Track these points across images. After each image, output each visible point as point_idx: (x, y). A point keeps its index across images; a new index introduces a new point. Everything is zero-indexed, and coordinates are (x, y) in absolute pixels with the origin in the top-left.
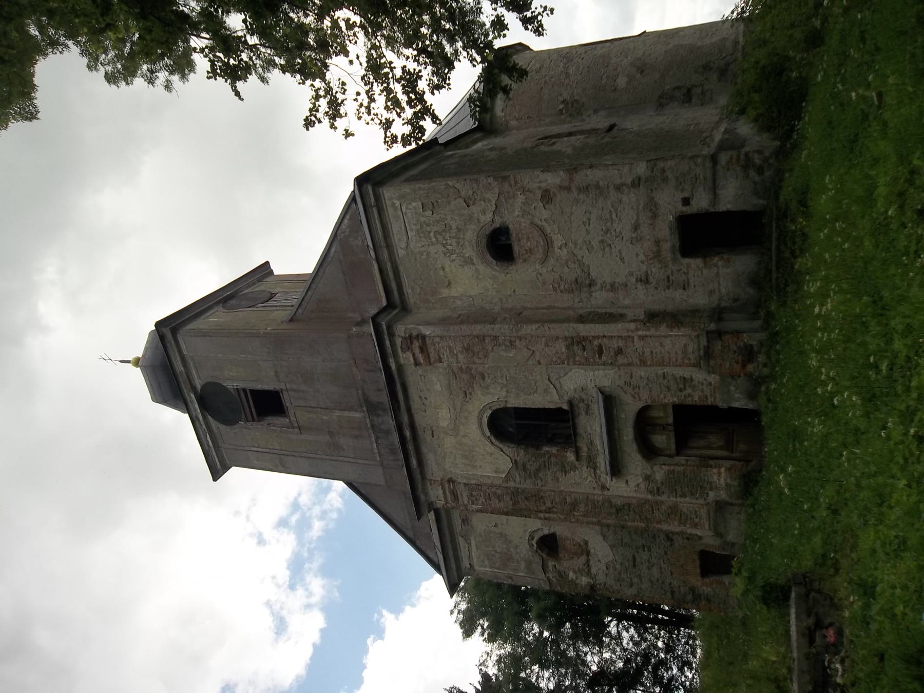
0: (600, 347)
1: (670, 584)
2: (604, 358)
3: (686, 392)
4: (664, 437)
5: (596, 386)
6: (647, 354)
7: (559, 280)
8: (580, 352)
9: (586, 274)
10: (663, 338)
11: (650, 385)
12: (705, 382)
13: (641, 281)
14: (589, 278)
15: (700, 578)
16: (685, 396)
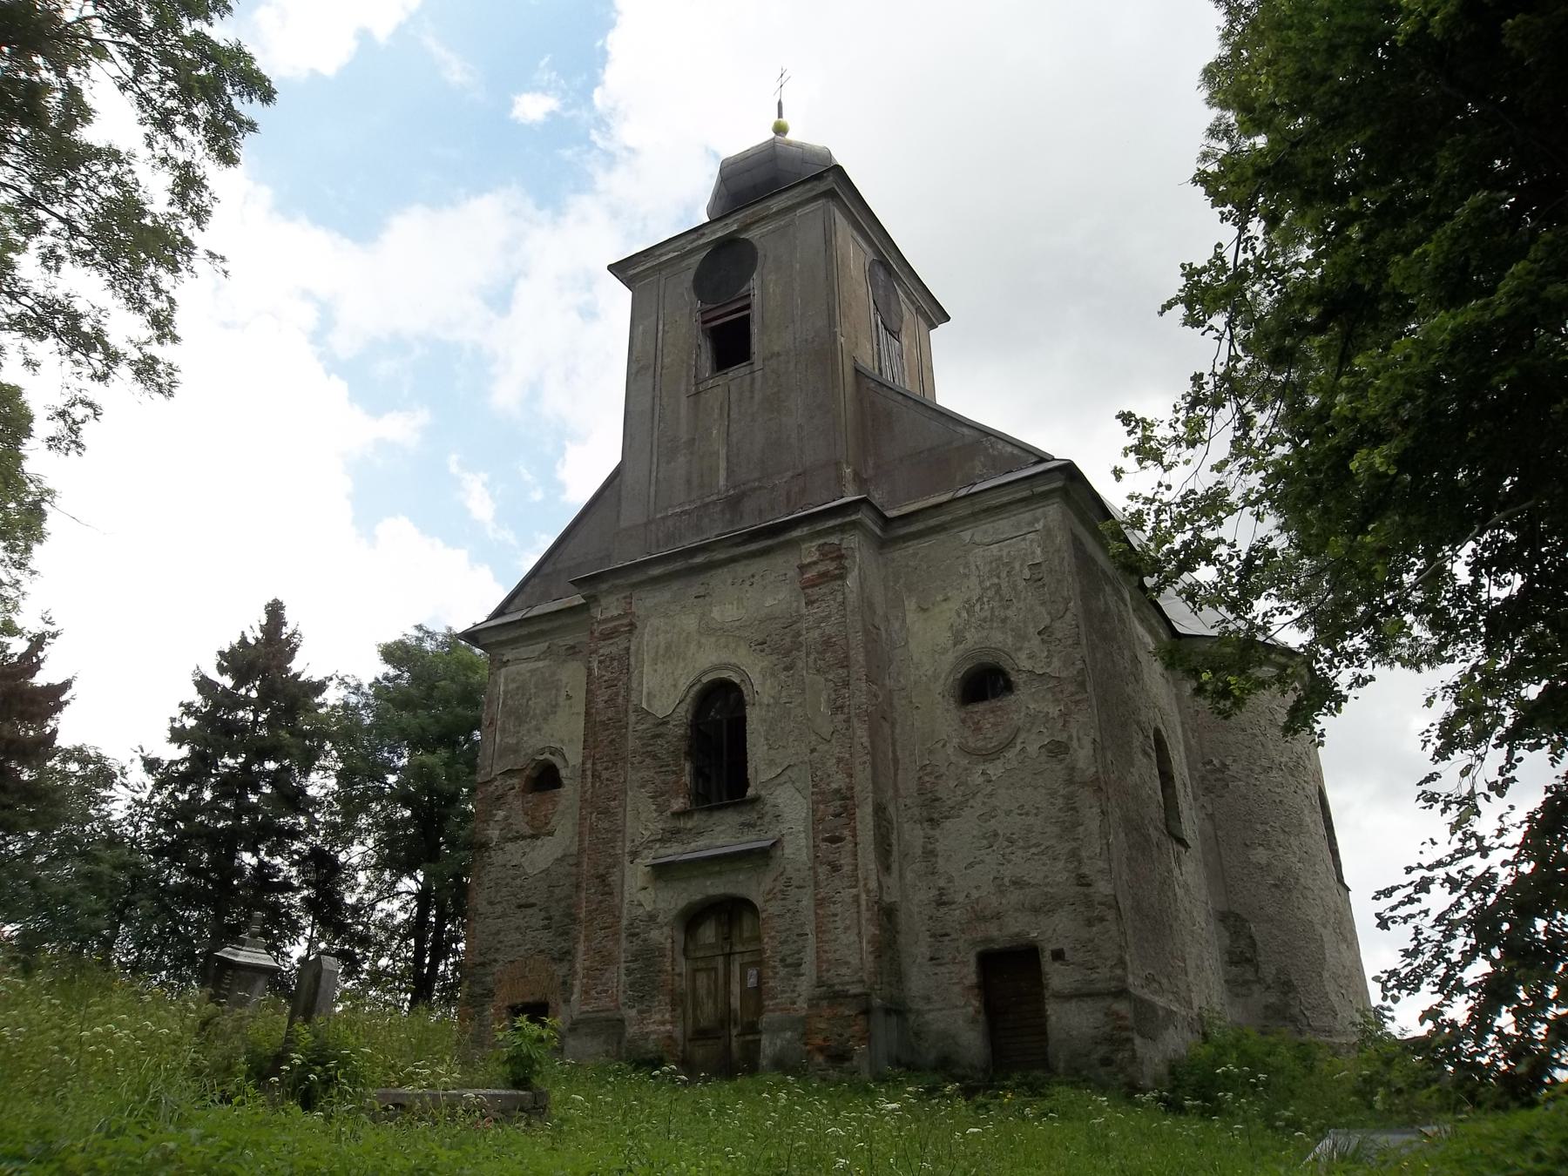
0: (840, 839)
1: (495, 961)
2: (824, 846)
4: (713, 940)
8: (831, 810)
13: (941, 895)
15: (507, 1004)
16: (775, 967)
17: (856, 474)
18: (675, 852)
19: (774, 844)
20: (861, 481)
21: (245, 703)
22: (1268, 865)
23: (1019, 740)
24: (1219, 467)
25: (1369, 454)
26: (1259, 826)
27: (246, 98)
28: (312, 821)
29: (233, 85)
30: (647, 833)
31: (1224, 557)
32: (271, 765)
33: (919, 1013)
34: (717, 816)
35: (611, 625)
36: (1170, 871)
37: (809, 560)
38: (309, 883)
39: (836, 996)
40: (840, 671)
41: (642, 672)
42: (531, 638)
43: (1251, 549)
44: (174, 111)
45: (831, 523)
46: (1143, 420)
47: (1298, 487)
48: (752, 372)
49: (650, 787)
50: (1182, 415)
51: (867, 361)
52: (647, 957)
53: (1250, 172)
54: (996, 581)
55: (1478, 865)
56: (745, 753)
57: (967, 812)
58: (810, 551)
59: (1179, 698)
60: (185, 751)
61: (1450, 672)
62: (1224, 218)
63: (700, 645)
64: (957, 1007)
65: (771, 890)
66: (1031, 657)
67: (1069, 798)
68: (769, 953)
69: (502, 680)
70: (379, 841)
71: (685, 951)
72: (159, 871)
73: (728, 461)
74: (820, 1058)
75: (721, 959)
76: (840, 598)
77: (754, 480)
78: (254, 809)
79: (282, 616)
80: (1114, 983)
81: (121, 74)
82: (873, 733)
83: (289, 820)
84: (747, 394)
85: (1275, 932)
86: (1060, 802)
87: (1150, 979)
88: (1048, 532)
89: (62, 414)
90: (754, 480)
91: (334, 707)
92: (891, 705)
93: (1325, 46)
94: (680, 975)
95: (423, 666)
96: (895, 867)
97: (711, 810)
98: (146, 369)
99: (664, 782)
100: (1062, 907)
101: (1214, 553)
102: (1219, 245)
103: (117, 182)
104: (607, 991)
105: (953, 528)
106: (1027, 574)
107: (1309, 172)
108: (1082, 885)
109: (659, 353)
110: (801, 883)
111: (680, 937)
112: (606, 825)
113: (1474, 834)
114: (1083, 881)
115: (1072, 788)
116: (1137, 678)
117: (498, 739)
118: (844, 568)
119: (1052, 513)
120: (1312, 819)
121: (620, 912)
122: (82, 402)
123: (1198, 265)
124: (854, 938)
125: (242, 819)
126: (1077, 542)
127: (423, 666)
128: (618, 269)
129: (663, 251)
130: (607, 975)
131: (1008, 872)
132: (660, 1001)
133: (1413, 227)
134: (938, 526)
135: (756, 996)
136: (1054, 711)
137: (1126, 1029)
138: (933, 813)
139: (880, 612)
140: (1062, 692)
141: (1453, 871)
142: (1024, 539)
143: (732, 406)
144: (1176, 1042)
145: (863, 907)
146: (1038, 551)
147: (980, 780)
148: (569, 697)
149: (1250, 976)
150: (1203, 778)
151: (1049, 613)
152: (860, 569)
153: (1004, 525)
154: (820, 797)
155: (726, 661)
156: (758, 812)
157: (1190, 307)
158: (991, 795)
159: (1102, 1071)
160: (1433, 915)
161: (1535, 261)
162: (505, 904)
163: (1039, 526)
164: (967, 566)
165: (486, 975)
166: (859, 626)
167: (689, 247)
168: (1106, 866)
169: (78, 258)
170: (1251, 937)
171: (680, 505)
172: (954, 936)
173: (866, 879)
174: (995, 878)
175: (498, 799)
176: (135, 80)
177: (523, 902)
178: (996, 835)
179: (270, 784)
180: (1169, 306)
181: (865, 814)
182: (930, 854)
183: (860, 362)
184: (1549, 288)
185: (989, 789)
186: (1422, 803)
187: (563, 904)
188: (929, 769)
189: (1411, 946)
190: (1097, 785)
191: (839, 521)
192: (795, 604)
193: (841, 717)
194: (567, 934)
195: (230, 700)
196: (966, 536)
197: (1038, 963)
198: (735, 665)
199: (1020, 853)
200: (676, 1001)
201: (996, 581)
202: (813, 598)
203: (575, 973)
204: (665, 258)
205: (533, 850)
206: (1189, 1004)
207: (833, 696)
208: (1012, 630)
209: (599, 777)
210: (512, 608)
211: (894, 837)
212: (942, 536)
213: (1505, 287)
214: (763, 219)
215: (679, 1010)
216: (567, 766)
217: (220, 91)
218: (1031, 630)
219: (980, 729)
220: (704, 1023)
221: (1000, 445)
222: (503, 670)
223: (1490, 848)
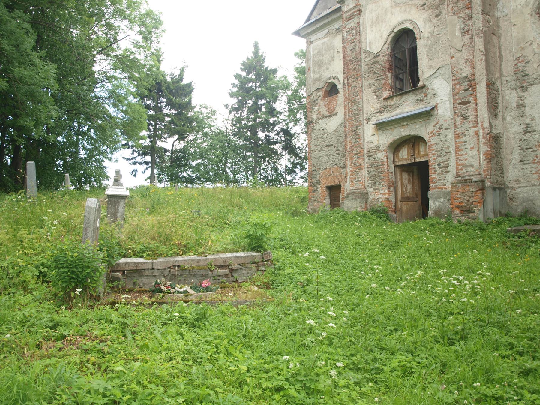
0: (468, 102)
1: (320, 169)
2: (459, 107)
3: (438, 169)
4: (407, 157)
5: (437, 104)
6: (464, 138)
7: (527, 61)
8: (463, 88)
9: (532, 82)
10: (477, 149)
11: (441, 143)
12: (446, 181)
13: (527, 127)
14: (529, 85)
16: (435, 168)
18: (386, 117)
19: (433, 109)
21: (251, 81)
30: (373, 109)
33: (512, 188)
34: (405, 97)
35: (350, 13)
60: (235, 100)
63: (392, 14)
64: (535, 185)
65: (432, 132)
69: (311, 50)
74: (457, 211)
82: (487, 43)
92: (498, 26)
94: (392, 173)
104: (360, 181)
110: (448, 127)
111: (391, 156)
112: (355, 108)
121: (364, 146)
124: (475, 152)
130: (360, 174)
132: (383, 185)
145: (481, 137)
154: (457, 81)
162: (321, 146)
165: (317, 174)
172: (535, 149)
173: (482, 122)
175: (315, 102)
177: (328, 144)
182: (521, 106)
188: (521, 59)
193: (467, 37)
209: (351, 86)
211: (500, 98)
220: (407, 194)
222: (312, 46)
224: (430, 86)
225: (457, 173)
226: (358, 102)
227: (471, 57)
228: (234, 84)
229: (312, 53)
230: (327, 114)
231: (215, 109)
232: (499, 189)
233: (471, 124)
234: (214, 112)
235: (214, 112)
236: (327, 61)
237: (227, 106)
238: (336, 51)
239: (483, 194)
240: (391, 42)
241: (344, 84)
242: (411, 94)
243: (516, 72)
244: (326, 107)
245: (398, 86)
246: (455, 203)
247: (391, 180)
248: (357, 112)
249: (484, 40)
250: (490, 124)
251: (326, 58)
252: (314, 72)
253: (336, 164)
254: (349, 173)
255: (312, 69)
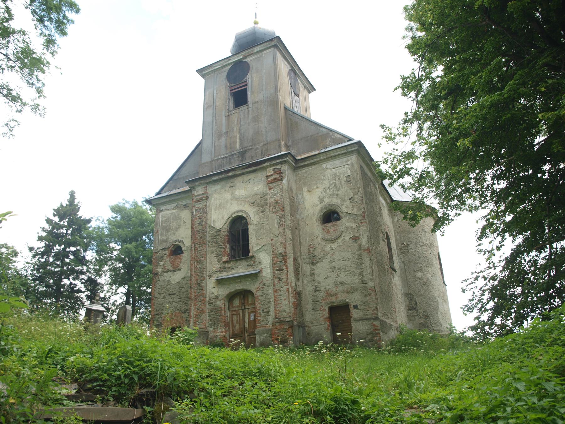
0: (282, 270)
1: (162, 313)
2: (276, 272)
4: (238, 305)
6: (280, 293)
8: (279, 260)
12: (267, 322)
13: (316, 288)
16: (260, 313)
17: (286, 144)
18: (224, 275)
19: (259, 272)
20: (287, 147)
21: (62, 227)
22: (421, 278)
23: (343, 236)
24: (414, 143)
25: (463, 141)
26: (418, 265)
27: (70, 12)
28: (88, 268)
29: (66, 7)
30: (214, 269)
31: (413, 174)
32: (73, 249)
33: (309, 327)
34: (239, 262)
35: (201, 196)
36: (391, 279)
37: (270, 174)
38: (88, 290)
39: (282, 322)
40: (281, 212)
41: (211, 213)
42: (170, 202)
43: (422, 171)
44: (44, 16)
45: (278, 161)
46: (388, 127)
47: (440, 151)
48: (248, 108)
49: (215, 253)
50: (401, 126)
51: (288, 105)
52: (216, 311)
53: (424, 46)
54: (335, 181)
55: (492, 272)
56: (248, 241)
57: (325, 260)
58: (270, 171)
59: (393, 222)
60: (43, 244)
61: (484, 212)
62: (415, 60)
63: (231, 204)
64: (321, 325)
65: (258, 287)
66: (347, 207)
67: (359, 255)
68: (258, 308)
69: (161, 217)
70: (111, 275)
71: (229, 308)
72: (36, 286)
73: (240, 139)
75: (241, 311)
76: (281, 187)
77: (250, 146)
78: (68, 264)
79: (74, 196)
80: (374, 315)
81: (26, 3)
82: (293, 234)
83: (80, 268)
84: (247, 116)
85: (423, 299)
86: (356, 256)
87: (385, 314)
88: (352, 165)
89: (7, 125)
90: (250, 146)
91: (95, 228)
92: (299, 224)
93: (450, 6)
94: (227, 316)
95: (125, 213)
96: (301, 279)
97: (237, 260)
98: (36, 108)
99: (220, 251)
100: (357, 291)
101: (410, 172)
102: (413, 69)
103: (24, 41)
105: (319, 163)
106: (345, 179)
107: (443, 47)
108: (364, 284)
109: (215, 101)
110: (269, 285)
111: (227, 304)
112: (200, 266)
113: (492, 262)
114: (364, 282)
115: (360, 252)
116: (381, 215)
117: (160, 238)
118: (282, 177)
119: (354, 158)
120: (436, 263)
121: (206, 296)
122: (13, 120)
123: (406, 76)
124: (287, 303)
125: (63, 268)
126: (361, 167)
127: (125, 213)
128: (200, 71)
129: (216, 65)
130: (202, 317)
131: (339, 280)
133: (478, 67)
134: (314, 162)
135: (254, 323)
136: (354, 225)
137: (378, 330)
138: (313, 260)
139: (294, 192)
140: (357, 219)
141: (485, 274)
142: (344, 167)
143: (241, 120)
144: (393, 334)
145: (290, 293)
146: (349, 171)
147: (329, 249)
148: (184, 222)
149: (415, 314)
150: (401, 249)
151: (353, 193)
152: (288, 177)
153: (337, 162)
154: (275, 255)
155: (241, 209)
156: (253, 261)
157: (403, 90)
158: (333, 254)
159: (370, 343)
160: (479, 288)
161: (516, 80)
163: (349, 163)
164: (324, 176)
166: (287, 197)
167: (225, 64)
168: (372, 277)
169: (9, 69)
170: (415, 301)
171: (223, 155)
172: (321, 301)
173: (291, 283)
174: (334, 282)
175: (161, 258)
176: (30, 5)
177: (171, 293)
178: (335, 267)
179: (73, 255)
180: (396, 89)
181: (290, 261)
182: (312, 274)
183: (286, 105)
184: (520, 89)
185: (332, 252)
186: (477, 252)
187: (185, 293)
188: (312, 246)
189: (471, 298)
190: (369, 251)
191: (280, 160)
192: (265, 189)
193: (282, 228)
194: (187, 303)
195: (58, 226)
196: (324, 166)
197: (349, 309)
198: (244, 211)
199: (343, 273)
200: (226, 325)
201: (335, 181)
202: (271, 187)
203: (191, 316)
204: (216, 68)
205: (173, 275)
206: (396, 322)
207: (279, 221)
208: (340, 198)
209: (197, 250)
210: (163, 191)
211: (300, 269)
212: (316, 166)
213: (506, 89)
214: (252, 54)
215: (227, 328)
216: (185, 247)
217: (60, 9)
218: (347, 198)
219: (329, 232)
220: (236, 332)
221: (336, 135)
222: (161, 214)
223: (496, 266)
224: (257, 257)
225: (275, 316)
226: (203, 263)
227: (284, 241)
228: (43, 228)
229: (161, 220)
230: (171, 269)
231: (18, 250)
232: (302, 326)
233: (284, 284)
234: (15, 254)
235: (15, 254)
236: (174, 228)
237: (31, 249)
238: (182, 221)
239: (293, 329)
240: (229, 223)
241: (191, 248)
242: (244, 261)
243: (309, 253)
244: (171, 263)
245: (233, 254)
246: (275, 337)
247: (227, 321)
248: (201, 270)
249: (292, 232)
250: (296, 284)
251: (174, 225)
252: (162, 234)
253: (178, 310)
254: (193, 316)
255: (160, 232)
